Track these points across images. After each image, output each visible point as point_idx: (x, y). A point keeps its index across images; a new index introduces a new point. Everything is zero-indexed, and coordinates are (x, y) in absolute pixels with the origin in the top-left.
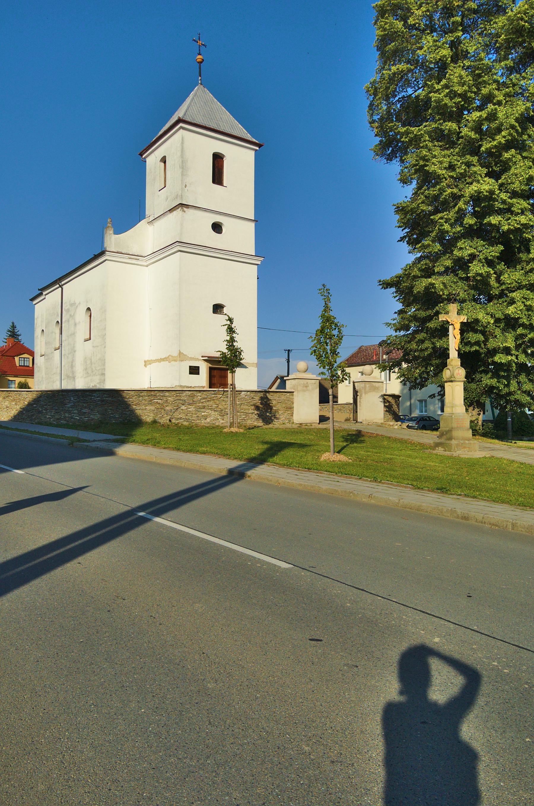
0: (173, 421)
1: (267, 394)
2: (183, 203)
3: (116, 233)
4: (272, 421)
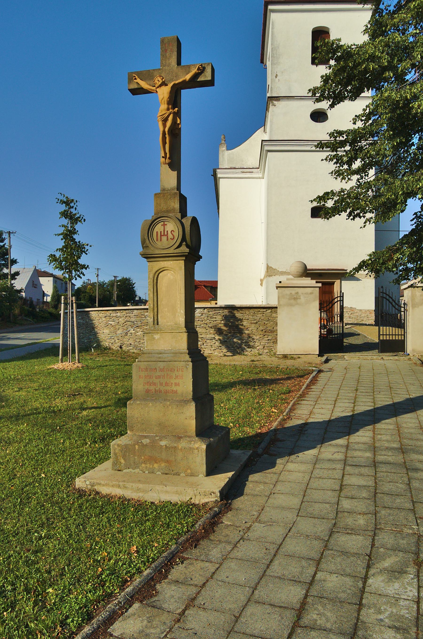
0: (124, 348)
1: (235, 312)
2: (274, 95)
3: (229, 148)
4: (243, 350)
